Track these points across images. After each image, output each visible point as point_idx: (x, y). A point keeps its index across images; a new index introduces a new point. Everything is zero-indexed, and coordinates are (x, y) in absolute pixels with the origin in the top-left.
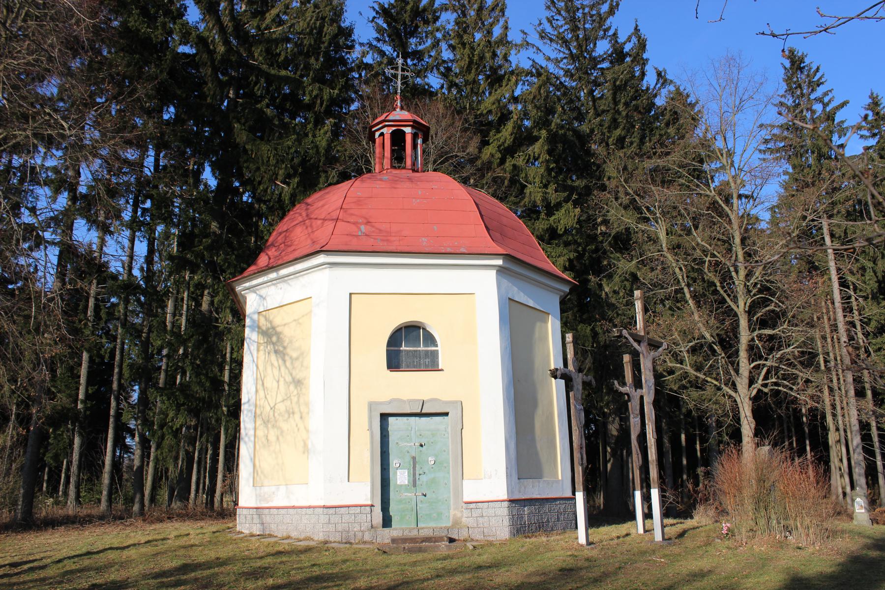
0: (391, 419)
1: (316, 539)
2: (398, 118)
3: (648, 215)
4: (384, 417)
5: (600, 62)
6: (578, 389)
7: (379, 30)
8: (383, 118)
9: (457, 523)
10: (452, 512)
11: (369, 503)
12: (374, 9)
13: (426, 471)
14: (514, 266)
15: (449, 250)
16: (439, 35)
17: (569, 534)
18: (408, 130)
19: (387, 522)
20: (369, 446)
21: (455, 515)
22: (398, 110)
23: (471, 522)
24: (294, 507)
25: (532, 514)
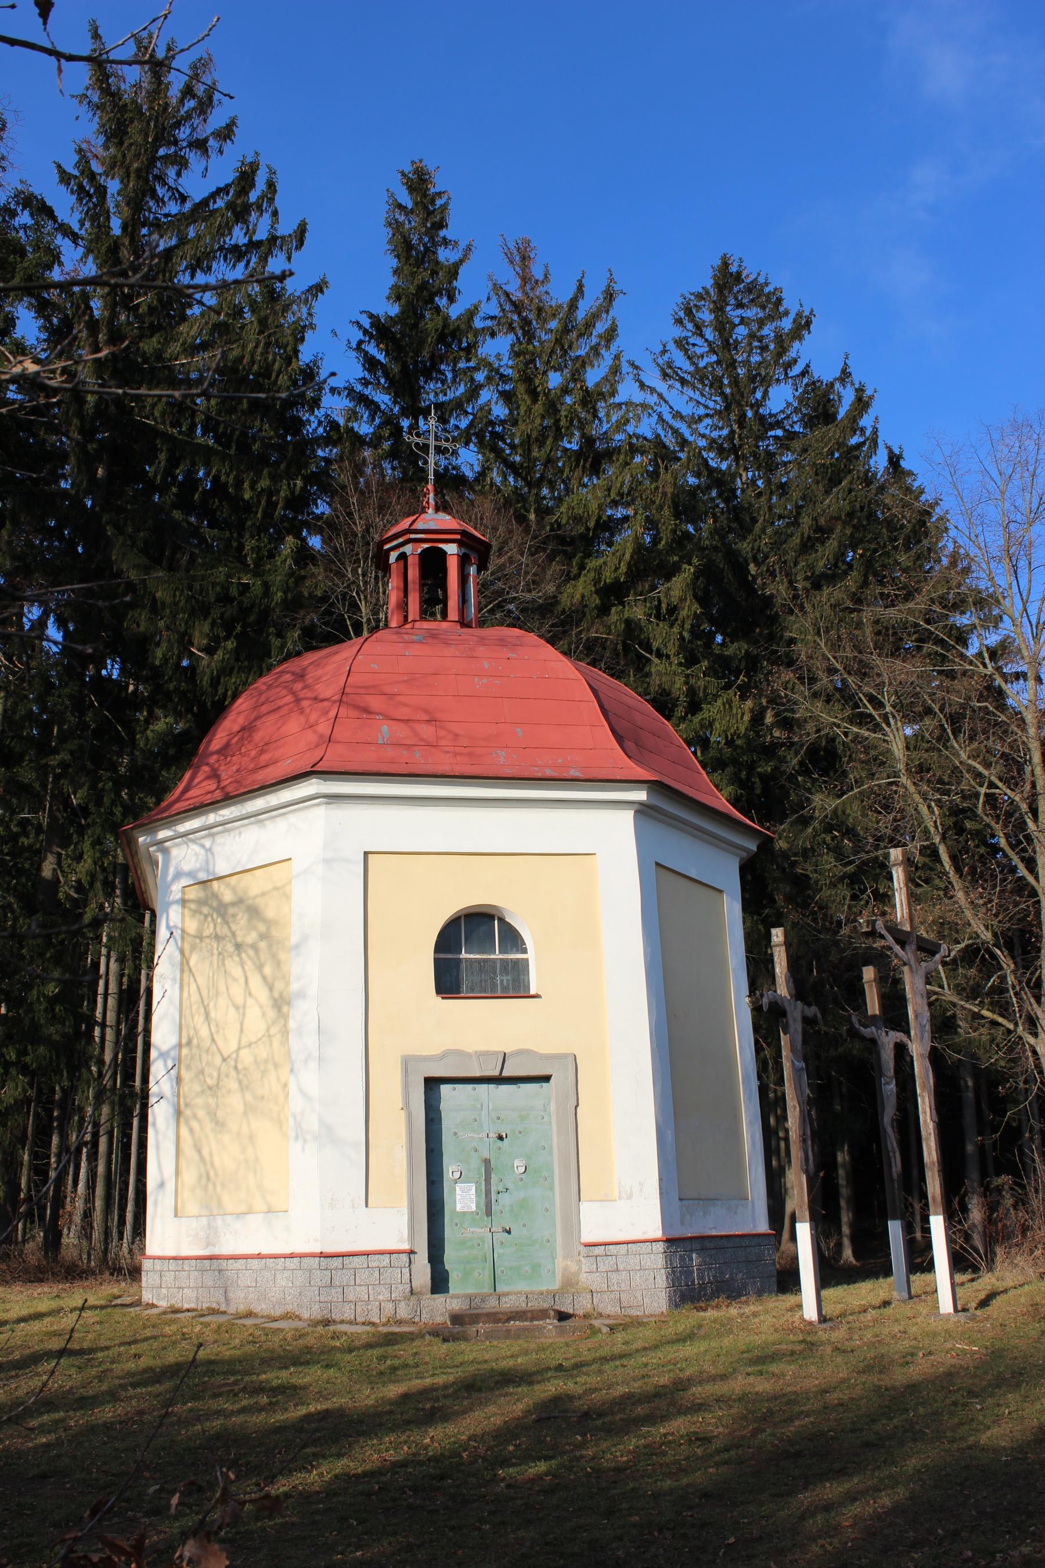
0: (445, 1089)
1: (306, 1315)
2: (432, 526)
3: (870, 709)
4: (432, 1084)
5: (772, 427)
6: (796, 1030)
7: (371, 364)
8: (405, 524)
9: (569, 1284)
10: (560, 1263)
11: (406, 1246)
12: (360, 327)
13: (510, 1186)
14: (666, 807)
15: (549, 773)
16: (480, 377)
17: (790, 1299)
18: (451, 549)
19: (439, 1282)
20: (403, 1139)
21: (565, 1269)
22: (430, 511)
23: (596, 1281)
24: (259, 1256)
25: (711, 1266)
